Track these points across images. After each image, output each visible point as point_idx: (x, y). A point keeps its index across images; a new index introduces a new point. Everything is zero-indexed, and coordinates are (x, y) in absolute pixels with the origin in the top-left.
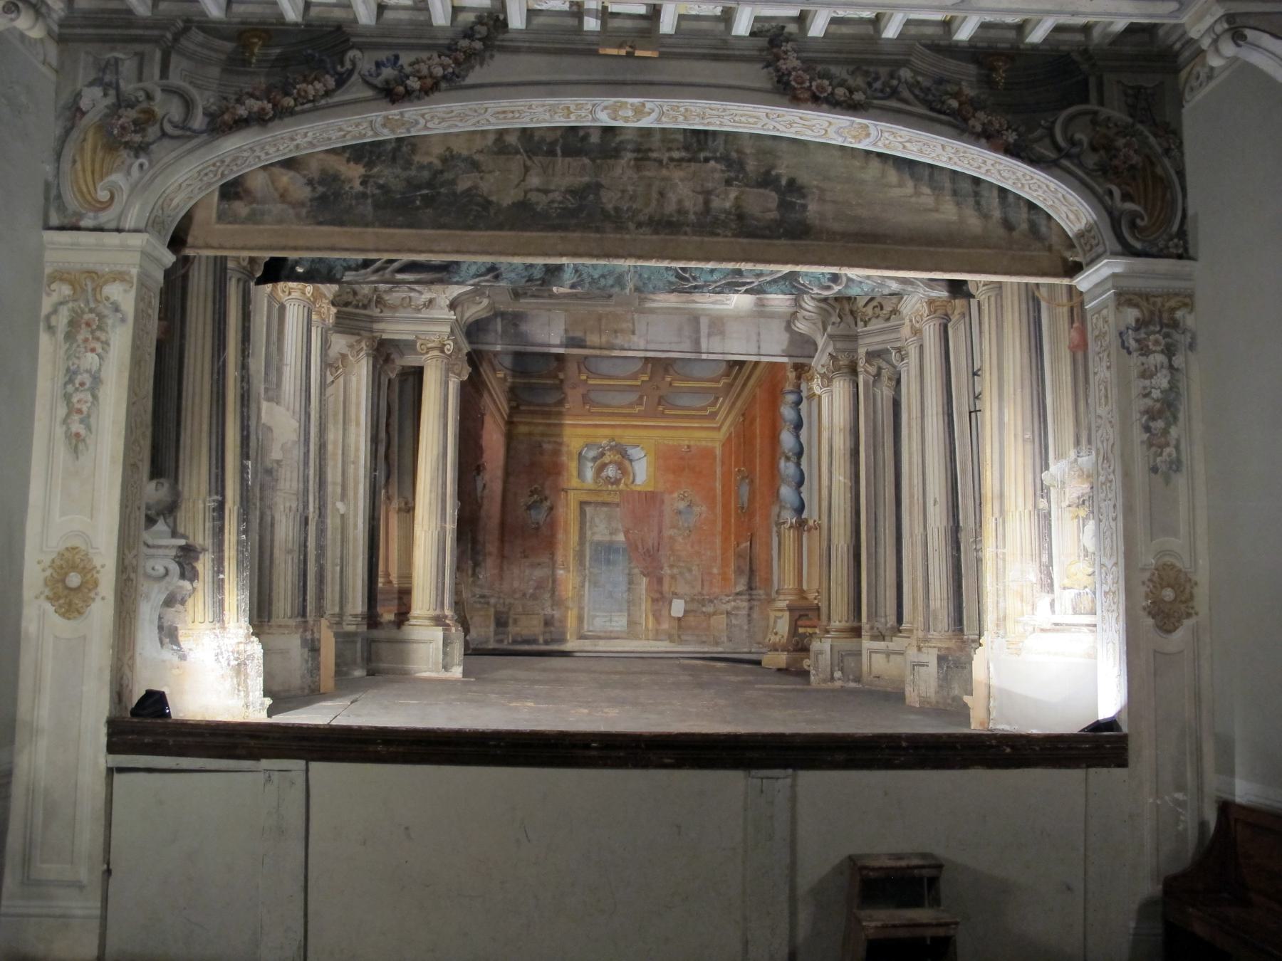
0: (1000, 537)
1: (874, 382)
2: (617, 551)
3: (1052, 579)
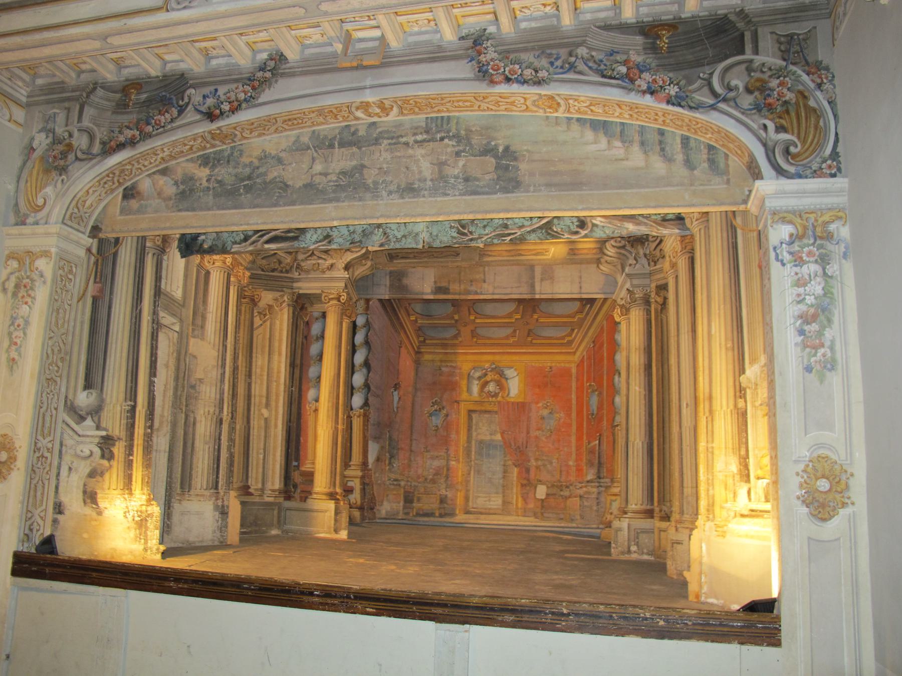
0: (710, 433)
1: (662, 309)
2: (495, 447)
3: (748, 470)
